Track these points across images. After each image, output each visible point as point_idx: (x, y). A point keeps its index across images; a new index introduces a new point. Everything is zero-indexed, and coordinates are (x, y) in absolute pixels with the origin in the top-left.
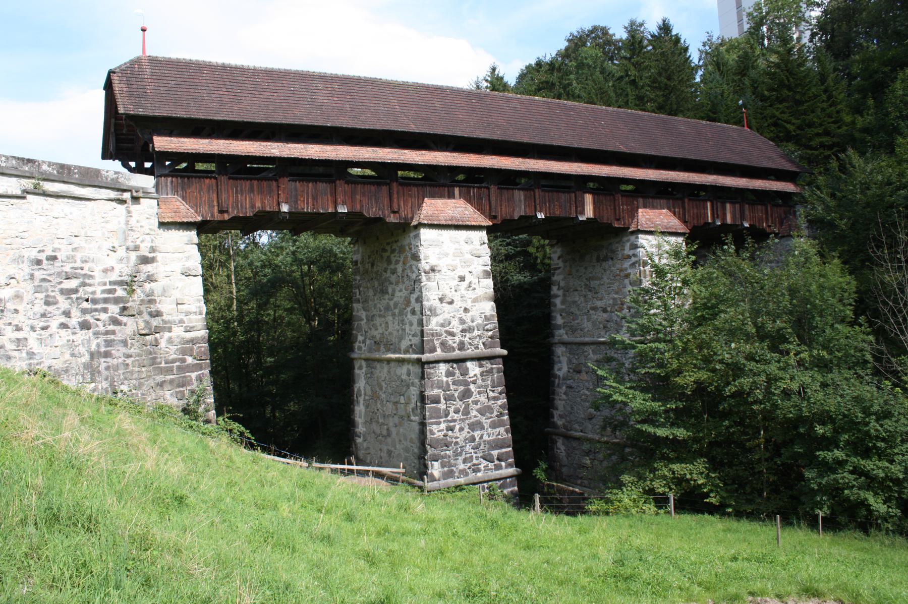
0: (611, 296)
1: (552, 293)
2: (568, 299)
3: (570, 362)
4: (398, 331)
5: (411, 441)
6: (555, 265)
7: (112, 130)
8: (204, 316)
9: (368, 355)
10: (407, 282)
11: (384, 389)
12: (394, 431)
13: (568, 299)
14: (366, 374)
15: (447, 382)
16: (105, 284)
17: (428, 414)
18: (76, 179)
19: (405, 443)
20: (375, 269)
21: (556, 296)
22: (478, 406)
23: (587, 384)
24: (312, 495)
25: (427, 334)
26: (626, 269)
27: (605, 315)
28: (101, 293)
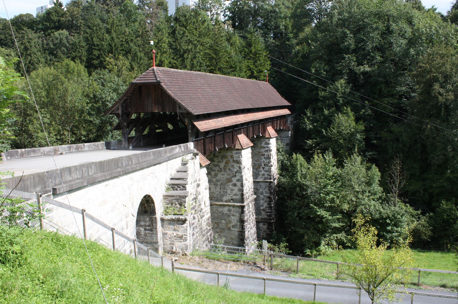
4: (220, 192)
24: (323, 275)
26: (263, 152)
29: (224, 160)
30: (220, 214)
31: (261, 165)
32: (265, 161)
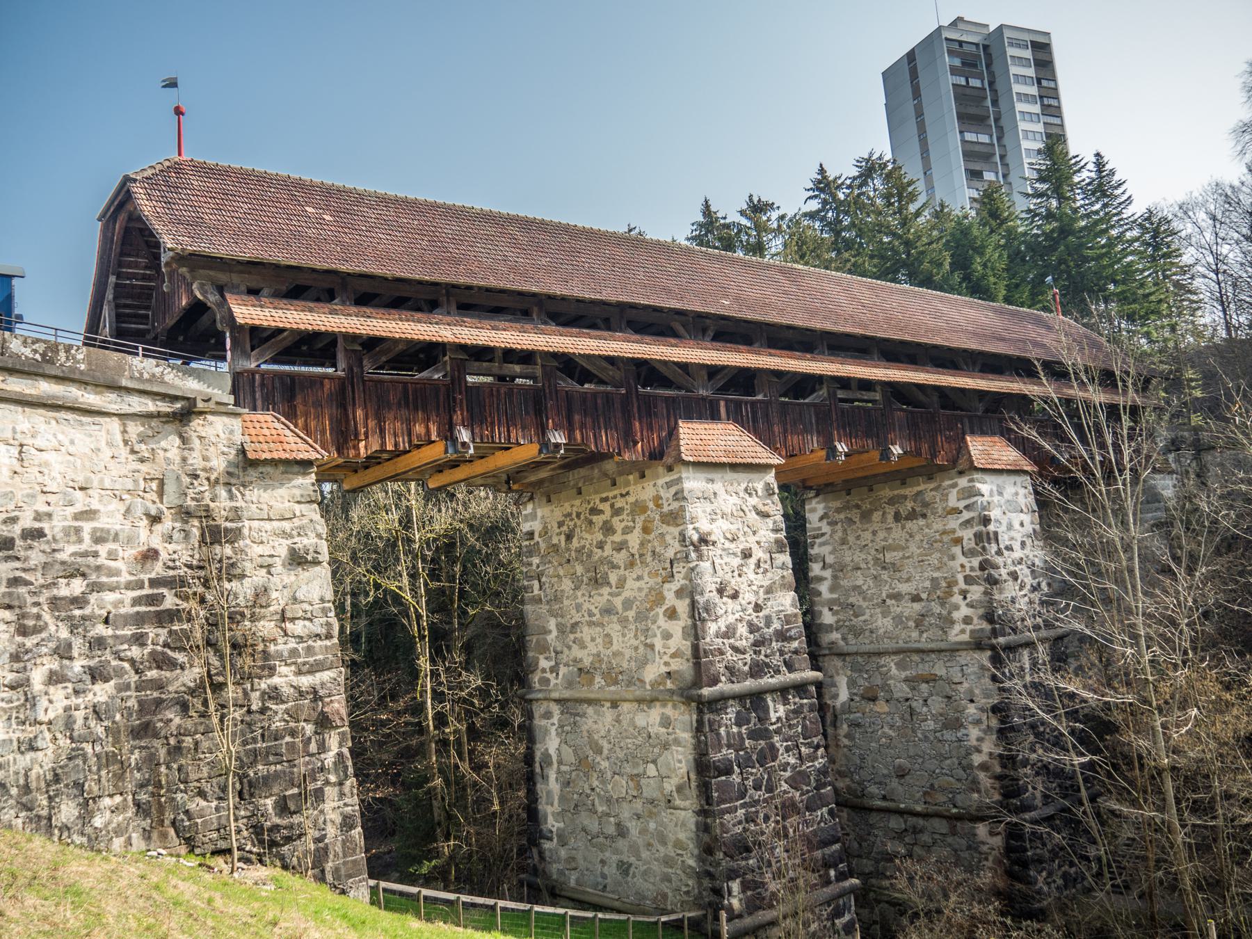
0: (926, 574)
1: (811, 574)
2: (844, 583)
3: (852, 683)
4: (636, 648)
5: (678, 844)
6: (815, 529)
7: (110, 295)
8: (335, 640)
9: (567, 694)
10: (654, 565)
11: (605, 752)
12: (633, 827)
13: (844, 583)
14: (562, 727)
15: (740, 733)
16: (140, 585)
17: (715, 795)
18: (82, 372)
19: (662, 849)
20: (575, 543)
21: (820, 579)
22: (788, 774)
23: (889, 718)
25: (705, 651)
26: (954, 531)
27: (917, 606)
28: (132, 606)
29: (637, 520)
30: (639, 741)
31: (956, 583)
32: (968, 565)
